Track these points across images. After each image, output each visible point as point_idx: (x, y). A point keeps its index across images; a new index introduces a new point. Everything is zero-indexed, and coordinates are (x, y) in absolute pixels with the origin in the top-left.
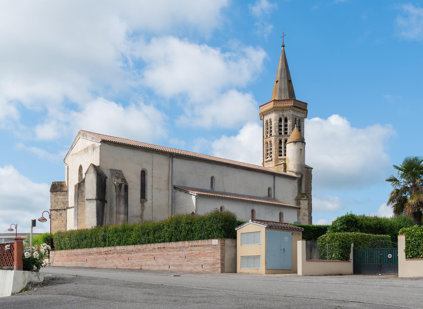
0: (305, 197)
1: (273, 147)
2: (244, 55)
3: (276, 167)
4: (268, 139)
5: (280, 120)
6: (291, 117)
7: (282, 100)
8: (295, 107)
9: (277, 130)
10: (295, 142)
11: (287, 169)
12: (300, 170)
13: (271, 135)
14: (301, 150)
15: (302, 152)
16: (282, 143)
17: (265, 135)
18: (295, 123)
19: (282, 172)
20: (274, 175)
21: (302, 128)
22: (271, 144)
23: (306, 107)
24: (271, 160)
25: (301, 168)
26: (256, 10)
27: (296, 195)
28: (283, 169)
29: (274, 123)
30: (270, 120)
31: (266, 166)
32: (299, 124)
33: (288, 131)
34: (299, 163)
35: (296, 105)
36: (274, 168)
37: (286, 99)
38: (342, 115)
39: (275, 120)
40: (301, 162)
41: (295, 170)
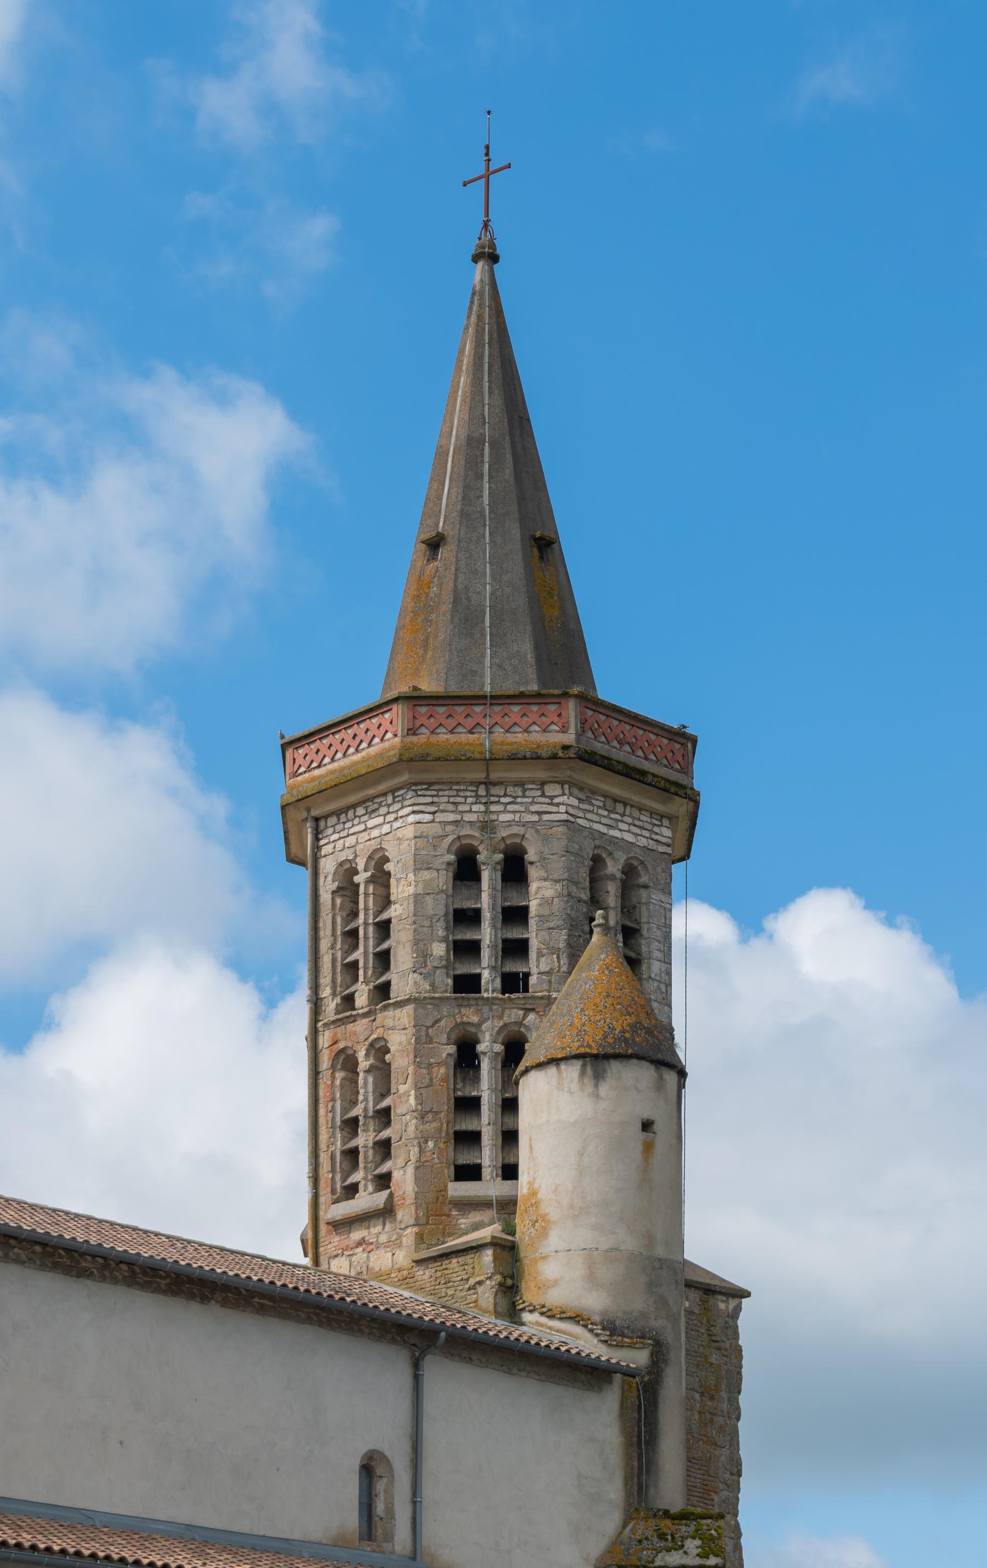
0: (692, 1545)
1: (405, 1099)
2: (131, 434)
3: (424, 1275)
4: (360, 1026)
5: (466, 869)
6: (559, 845)
7: (480, 699)
8: (589, 758)
9: (439, 949)
10: (596, 1061)
11: (529, 1294)
12: (639, 1303)
13: (383, 991)
14: (647, 1126)
15: (655, 1146)
16: (485, 1065)
17: (326, 992)
18: (595, 901)
19: (490, 1324)
20: (416, 1339)
21: (649, 946)
22: (383, 1071)
23: (687, 769)
24: (387, 1212)
25: (651, 1286)
26: (226, 107)
27: (609, 1522)
28: (487, 1295)
29: (412, 891)
30: (379, 862)
31: (340, 1266)
32: (628, 908)
33: (537, 965)
34: (630, 1244)
35: (600, 747)
36: (406, 1281)
37: (510, 687)
38: (717, 903)
39: (420, 864)
40: (649, 1238)
41: (594, 1302)
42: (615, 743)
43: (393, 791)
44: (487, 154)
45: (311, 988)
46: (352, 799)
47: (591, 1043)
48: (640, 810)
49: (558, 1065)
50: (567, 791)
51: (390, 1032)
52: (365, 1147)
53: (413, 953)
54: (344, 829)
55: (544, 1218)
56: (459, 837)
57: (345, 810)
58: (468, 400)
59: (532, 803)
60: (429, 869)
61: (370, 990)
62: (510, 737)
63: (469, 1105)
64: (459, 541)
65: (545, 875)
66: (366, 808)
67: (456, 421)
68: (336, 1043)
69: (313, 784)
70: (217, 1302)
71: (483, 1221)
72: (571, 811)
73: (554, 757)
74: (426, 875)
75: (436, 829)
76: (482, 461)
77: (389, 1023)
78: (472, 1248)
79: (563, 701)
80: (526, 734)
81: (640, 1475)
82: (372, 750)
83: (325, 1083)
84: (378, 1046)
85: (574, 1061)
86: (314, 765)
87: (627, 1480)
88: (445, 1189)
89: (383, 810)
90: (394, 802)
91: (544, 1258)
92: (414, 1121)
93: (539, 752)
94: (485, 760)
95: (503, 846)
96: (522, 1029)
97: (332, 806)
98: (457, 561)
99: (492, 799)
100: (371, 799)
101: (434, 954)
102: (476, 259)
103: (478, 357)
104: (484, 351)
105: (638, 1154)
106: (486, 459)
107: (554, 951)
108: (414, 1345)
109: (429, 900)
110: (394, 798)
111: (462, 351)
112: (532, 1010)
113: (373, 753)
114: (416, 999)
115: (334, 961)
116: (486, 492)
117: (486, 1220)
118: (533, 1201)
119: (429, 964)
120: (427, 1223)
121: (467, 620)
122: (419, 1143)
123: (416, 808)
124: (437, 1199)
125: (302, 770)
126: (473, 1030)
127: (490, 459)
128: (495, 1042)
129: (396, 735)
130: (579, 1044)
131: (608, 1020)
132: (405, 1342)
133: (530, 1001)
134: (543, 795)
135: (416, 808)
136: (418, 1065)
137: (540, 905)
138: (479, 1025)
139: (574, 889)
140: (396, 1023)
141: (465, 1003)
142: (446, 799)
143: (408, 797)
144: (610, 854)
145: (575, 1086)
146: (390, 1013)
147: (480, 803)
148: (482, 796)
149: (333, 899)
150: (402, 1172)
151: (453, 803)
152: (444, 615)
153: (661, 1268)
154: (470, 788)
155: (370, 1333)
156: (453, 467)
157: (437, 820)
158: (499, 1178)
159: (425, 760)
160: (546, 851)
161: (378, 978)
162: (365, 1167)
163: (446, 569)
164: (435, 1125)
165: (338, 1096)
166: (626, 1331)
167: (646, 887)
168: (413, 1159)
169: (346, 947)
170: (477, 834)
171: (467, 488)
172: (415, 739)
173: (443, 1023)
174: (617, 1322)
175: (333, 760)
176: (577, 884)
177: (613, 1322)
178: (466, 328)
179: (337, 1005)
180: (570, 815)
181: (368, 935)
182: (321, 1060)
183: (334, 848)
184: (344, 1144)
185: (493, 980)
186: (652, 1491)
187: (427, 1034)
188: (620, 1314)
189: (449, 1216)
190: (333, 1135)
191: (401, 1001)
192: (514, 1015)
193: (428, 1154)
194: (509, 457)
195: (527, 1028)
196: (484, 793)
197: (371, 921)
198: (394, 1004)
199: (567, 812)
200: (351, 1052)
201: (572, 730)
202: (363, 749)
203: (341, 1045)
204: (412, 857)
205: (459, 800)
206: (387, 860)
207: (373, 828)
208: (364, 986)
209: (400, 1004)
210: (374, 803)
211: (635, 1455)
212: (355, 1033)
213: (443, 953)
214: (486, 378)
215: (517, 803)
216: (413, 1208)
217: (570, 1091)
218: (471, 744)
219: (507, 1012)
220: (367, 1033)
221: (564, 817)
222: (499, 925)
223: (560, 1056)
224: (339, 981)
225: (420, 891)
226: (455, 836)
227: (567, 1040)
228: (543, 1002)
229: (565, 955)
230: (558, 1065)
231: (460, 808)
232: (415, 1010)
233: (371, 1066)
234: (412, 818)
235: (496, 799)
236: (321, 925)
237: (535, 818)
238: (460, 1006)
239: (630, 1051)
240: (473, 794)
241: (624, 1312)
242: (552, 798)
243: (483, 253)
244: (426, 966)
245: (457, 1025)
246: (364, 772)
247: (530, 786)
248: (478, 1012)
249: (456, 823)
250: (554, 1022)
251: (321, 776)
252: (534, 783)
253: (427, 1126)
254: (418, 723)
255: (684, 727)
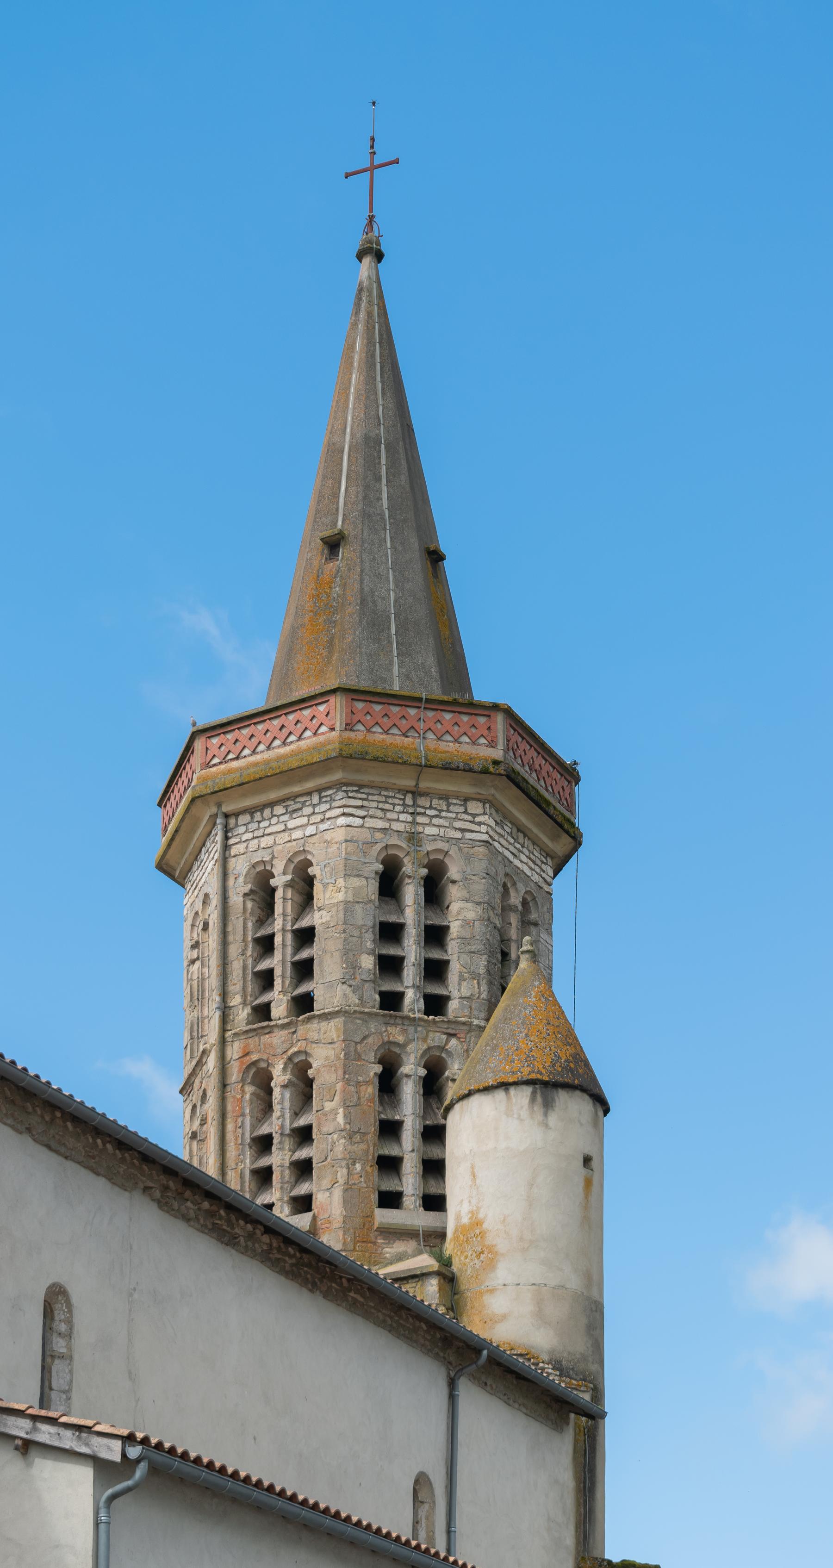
1: (331, 1115)
4: (278, 1038)
5: (389, 884)
6: (480, 866)
9: (368, 962)
13: (304, 1004)
17: (236, 1000)
22: (304, 1088)
29: (340, 897)
33: (460, 988)
39: (351, 871)
42: (527, 768)
43: (320, 790)
44: (372, 147)
45: (220, 995)
46: (273, 795)
47: (541, 1069)
48: (534, 844)
49: (507, 1090)
50: (488, 811)
51: (314, 1045)
52: (282, 1166)
53: (343, 962)
54: (259, 828)
55: (491, 1249)
56: (386, 847)
57: (261, 808)
58: (363, 398)
59: (456, 819)
60: (358, 876)
61: (288, 1000)
62: (442, 746)
63: (390, 1129)
64: (363, 542)
65: (467, 896)
66: (286, 807)
67: (349, 418)
68: (247, 1054)
69: (233, 776)
70: (321, 1292)
71: (406, 1252)
72: (491, 833)
73: (485, 771)
74: (357, 882)
75: (365, 835)
76: (380, 463)
77: (313, 1035)
78: (414, 1277)
79: (492, 713)
80: (457, 745)
81: (585, 1522)
82: (258, 758)
83: (234, 1097)
84: (296, 1060)
85: (525, 1087)
86: (231, 756)
87: (577, 1528)
88: (371, 1216)
89: (307, 810)
90: (320, 803)
91: (492, 1291)
92: (343, 1141)
93: (472, 764)
94: (421, 766)
95: (426, 861)
96: (443, 1055)
97: (248, 802)
98: (362, 562)
99: (419, 810)
100: (294, 797)
101: (363, 966)
102: (360, 257)
103: (371, 355)
104: (375, 349)
105: (580, 1189)
106: (383, 461)
107: (475, 976)
108: (450, 1363)
109: (358, 908)
110: (320, 798)
111: (351, 347)
112: (454, 1035)
113: (305, 747)
114: (346, 1012)
115: (245, 968)
116: (385, 496)
117: (410, 1251)
118: (478, 1232)
119: (358, 976)
120: (354, 1250)
121: (374, 625)
122: (348, 1164)
123: (347, 810)
124: (364, 1225)
125: (216, 761)
126: (397, 1050)
127: (387, 461)
128: (418, 1065)
129: (333, 729)
130: (529, 1069)
131: (553, 1048)
132: (444, 1358)
133: (453, 1026)
134: (466, 812)
135: (347, 810)
136: (348, 1082)
137: (462, 926)
138: (403, 1046)
139: (491, 914)
140: (322, 1037)
141: (392, 1021)
142: (375, 804)
143: (338, 798)
144: (514, 884)
145: (525, 1113)
146: (314, 1025)
147: (407, 813)
148: (409, 806)
149: (244, 902)
150: (327, 1194)
151: (382, 809)
152: (350, 616)
153: (596, 1311)
154: (398, 796)
155: (423, 1345)
156: (349, 466)
157: (367, 825)
158: (422, 1208)
159: (363, 759)
160: (469, 871)
161: (294, 990)
162: (282, 1188)
163: (349, 569)
164: (363, 1146)
165: (248, 1111)
166: (571, 1372)
167: (536, 924)
168: (341, 1181)
169: (255, 955)
170: (404, 845)
171: (367, 487)
172: (352, 735)
173: (370, 1040)
174: (564, 1363)
175: (254, 752)
176: (493, 908)
177: (560, 1362)
178: (354, 325)
179: (248, 1014)
180: (490, 836)
181: (283, 942)
182: (229, 1072)
183: (247, 847)
184: (252, 1163)
185: (418, 1000)
186: (591, 1541)
187: (356, 1050)
188: (565, 1355)
189: (375, 1243)
190: (243, 1153)
191: (329, 1013)
192: (437, 1038)
193: (356, 1176)
194: (404, 463)
195: (449, 1053)
196: (411, 803)
197: (289, 928)
198: (319, 1016)
199: (487, 833)
200: (263, 1065)
201: (501, 745)
202: (292, 742)
203: (254, 1057)
204: (343, 861)
205: (387, 807)
206: (311, 864)
207: (294, 828)
208: (281, 996)
209: (326, 1017)
210: (296, 803)
211: (582, 1501)
212: (271, 1045)
213: (371, 966)
214: (379, 378)
215: (441, 817)
216: (341, 1233)
217: (520, 1119)
218: (406, 748)
219: (431, 1035)
220: (285, 1046)
221: (485, 837)
222: (422, 944)
223: (511, 1080)
224: (250, 989)
225: (350, 899)
226: (384, 845)
227: (516, 1065)
228: (464, 1028)
229: (485, 981)
230: (507, 1090)
231: (389, 815)
232: (345, 1023)
233: (290, 1081)
234: (342, 821)
235: (422, 811)
236: (230, 928)
237: (458, 835)
238: (386, 1024)
239: (576, 1082)
240: (401, 802)
241: (569, 1353)
242: (474, 816)
243: (371, 249)
244: (355, 978)
245: (384, 1044)
246: (296, 765)
247: (454, 801)
248: (404, 1031)
249: (384, 830)
250: (497, 1046)
251: (240, 769)
252: (457, 798)
253: (355, 1147)
254: (356, 718)
255: (575, 763)
